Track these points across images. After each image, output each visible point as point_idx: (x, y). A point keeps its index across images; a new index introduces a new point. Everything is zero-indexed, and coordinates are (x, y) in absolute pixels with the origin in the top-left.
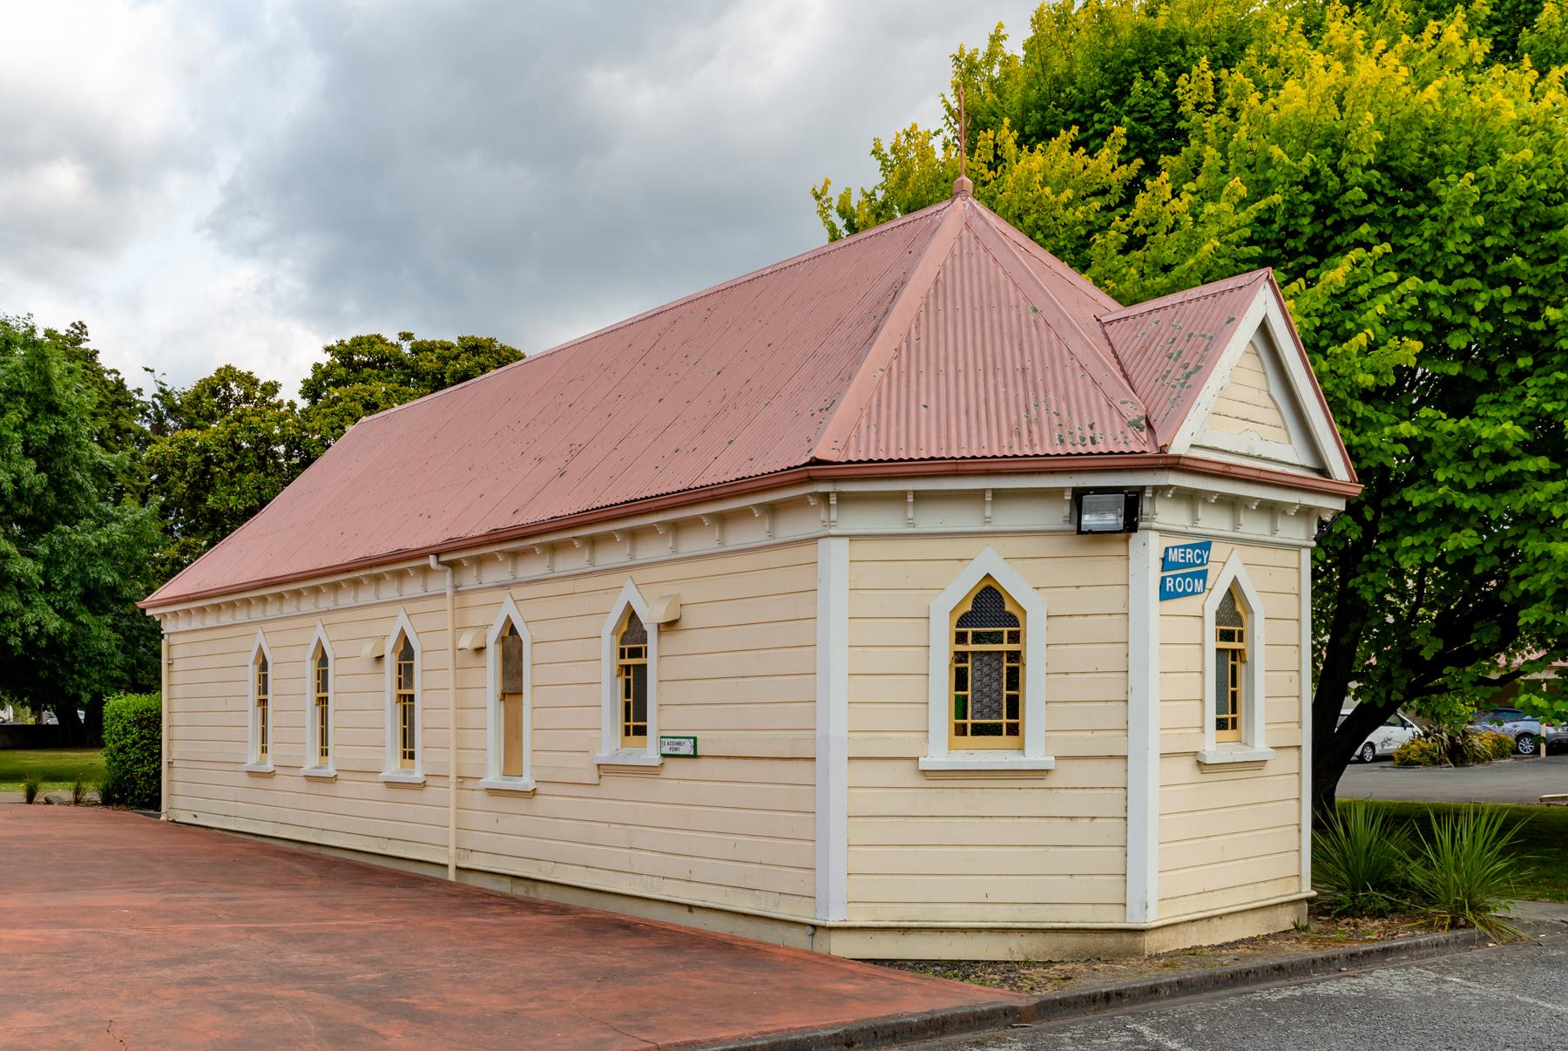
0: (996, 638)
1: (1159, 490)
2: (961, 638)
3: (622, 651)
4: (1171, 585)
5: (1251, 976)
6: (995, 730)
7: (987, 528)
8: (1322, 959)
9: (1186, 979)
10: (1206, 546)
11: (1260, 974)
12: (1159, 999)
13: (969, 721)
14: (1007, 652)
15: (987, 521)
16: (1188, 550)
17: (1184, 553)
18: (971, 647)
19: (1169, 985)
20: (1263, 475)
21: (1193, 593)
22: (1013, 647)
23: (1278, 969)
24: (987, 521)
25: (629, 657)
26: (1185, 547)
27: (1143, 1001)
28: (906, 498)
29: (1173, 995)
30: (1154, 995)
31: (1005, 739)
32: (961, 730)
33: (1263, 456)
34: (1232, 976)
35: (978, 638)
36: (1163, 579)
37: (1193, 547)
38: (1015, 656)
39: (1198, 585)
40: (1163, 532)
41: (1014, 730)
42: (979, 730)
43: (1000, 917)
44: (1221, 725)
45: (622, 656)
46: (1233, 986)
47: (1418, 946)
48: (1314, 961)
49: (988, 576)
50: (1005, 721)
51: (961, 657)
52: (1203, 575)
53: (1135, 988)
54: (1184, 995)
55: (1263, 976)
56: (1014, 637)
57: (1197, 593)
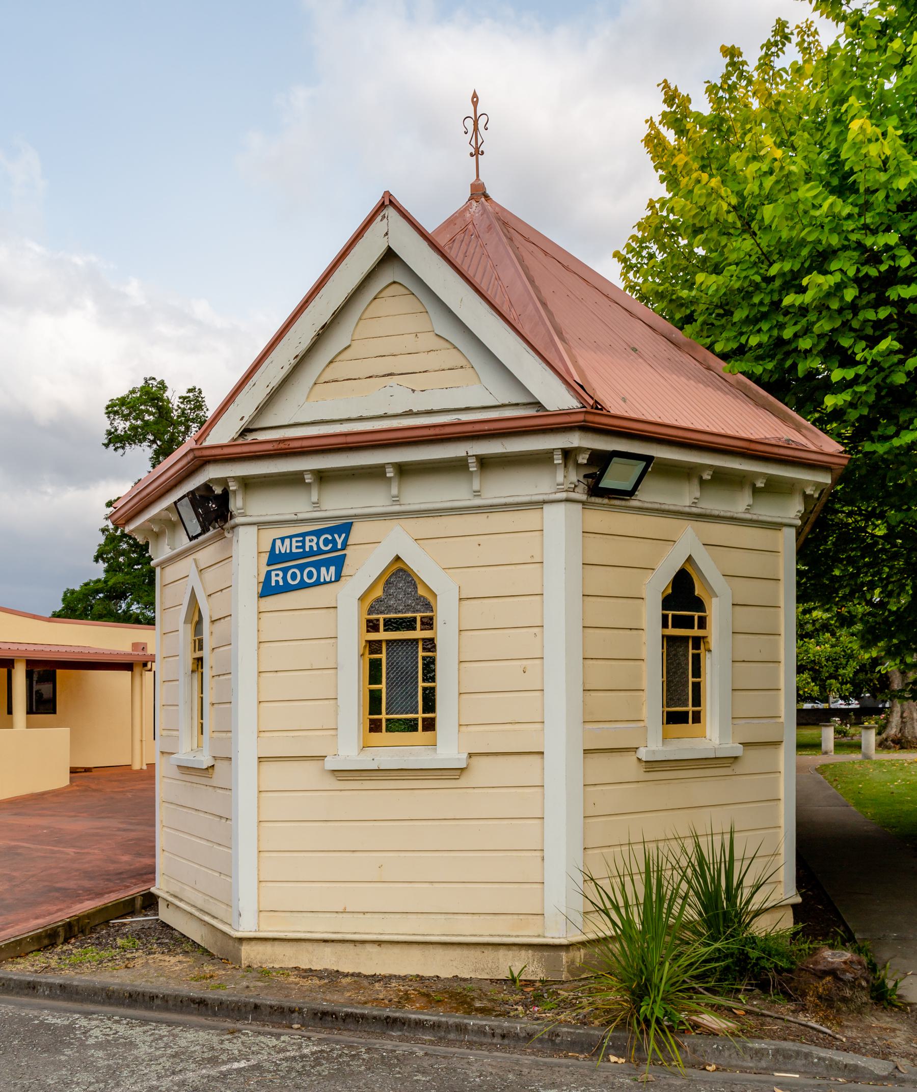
0: (409, 624)
1: (247, 484)
2: (372, 626)
3: (665, 618)
4: (280, 579)
5: (158, 1002)
6: (411, 726)
7: (477, 502)
8: (271, 1007)
9: (71, 986)
10: (345, 528)
11: (170, 1003)
12: (35, 997)
13: (384, 716)
14: (423, 639)
15: (477, 494)
16: (307, 538)
17: (303, 542)
18: (382, 635)
19: (51, 986)
20: (350, 439)
21: (318, 583)
22: (427, 634)
23: (199, 1003)
24: (477, 494)
25: (673, 627)
26: (304, 535)
27: (18, 993)
28: (551, 459)
29: (51, 997)
30: (31, 991)
31: (420, 735)
32: (375, 727)
33: (415, 410)
34: (130, 996)
35: (390, 625)
36: (268, 574)
37: (318, 533)
38: (430, 645)
39: (327, 574)
40: (261, 525)
41: (430, 725)
42: (394, 726)
43: (436, 930)
44: (674, 719)
45: (665, 625)
46: (130, 1006)
47: (461, 1029)
48: (256, 1007)
49: (398, 559)
50: (420, 715)
51: (374, 646)
52: (339, 563)
53: (10, 979)
54: (65, 1000)
55: (175, 1005)
56: (428, 624)
57: (325, 583)
